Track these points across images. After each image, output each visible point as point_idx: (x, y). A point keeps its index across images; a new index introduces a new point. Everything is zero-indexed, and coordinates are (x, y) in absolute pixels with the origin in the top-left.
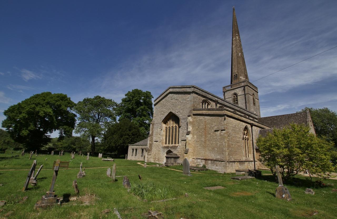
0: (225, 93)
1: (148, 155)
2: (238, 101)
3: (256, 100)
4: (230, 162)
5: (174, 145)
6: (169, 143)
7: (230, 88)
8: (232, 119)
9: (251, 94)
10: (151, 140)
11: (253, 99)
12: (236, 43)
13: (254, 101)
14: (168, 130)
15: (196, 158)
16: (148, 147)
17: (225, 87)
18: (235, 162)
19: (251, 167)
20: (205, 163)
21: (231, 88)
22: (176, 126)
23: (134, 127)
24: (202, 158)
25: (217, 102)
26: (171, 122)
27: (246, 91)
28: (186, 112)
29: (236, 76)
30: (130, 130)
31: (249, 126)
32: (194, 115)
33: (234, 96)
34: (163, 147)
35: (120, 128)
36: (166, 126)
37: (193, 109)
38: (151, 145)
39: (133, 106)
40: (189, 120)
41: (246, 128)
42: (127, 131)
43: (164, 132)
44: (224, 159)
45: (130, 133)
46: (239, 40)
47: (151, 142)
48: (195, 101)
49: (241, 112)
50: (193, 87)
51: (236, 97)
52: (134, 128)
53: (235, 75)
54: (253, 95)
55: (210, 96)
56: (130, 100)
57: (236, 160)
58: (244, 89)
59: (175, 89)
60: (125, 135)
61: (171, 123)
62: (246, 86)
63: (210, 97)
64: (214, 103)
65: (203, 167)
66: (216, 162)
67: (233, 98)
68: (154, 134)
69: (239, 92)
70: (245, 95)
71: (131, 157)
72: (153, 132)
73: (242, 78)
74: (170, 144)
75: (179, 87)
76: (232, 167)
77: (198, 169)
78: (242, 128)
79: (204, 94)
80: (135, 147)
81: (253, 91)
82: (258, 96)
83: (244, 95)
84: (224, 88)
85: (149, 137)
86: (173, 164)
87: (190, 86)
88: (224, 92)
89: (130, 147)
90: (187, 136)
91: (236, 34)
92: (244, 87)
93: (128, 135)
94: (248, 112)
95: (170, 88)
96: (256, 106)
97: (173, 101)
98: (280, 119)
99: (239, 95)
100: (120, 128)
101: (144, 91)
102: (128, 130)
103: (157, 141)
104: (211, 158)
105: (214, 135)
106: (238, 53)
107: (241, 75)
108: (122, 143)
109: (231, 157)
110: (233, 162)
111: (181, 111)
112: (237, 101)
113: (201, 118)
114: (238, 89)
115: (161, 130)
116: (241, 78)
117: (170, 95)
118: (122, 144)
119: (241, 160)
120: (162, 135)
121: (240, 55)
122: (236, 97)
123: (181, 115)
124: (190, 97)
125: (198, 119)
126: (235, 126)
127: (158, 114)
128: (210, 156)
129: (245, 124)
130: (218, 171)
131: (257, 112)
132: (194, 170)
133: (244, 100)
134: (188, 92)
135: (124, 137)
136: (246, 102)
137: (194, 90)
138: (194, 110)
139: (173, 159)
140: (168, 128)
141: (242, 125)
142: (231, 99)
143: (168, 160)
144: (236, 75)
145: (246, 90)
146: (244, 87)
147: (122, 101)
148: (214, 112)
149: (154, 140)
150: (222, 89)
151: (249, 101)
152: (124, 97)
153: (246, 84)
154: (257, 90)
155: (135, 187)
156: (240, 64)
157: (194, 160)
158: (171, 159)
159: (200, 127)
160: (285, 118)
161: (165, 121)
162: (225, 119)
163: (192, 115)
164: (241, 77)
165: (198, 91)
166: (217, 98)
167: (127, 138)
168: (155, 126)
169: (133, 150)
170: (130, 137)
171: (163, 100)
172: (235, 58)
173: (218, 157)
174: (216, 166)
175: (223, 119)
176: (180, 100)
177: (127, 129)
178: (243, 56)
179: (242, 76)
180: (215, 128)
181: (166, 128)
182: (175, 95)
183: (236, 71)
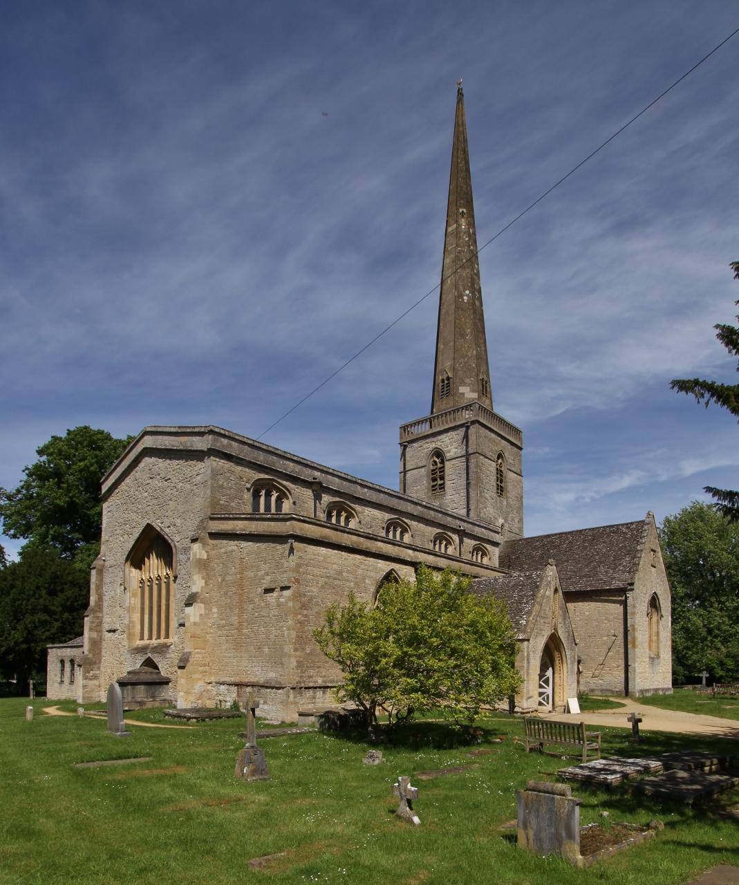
0: (405, 447)
1: (86, 678)
2: (446, 478)
3: (512, 475)
4: (306, 688)
5: (162, 640)
6: (150, 638)
7: (425, 429)
9: (489, 454)
10: (98, 627)
11: (499, 472)
12: (457, 246)
13: (500, 476)
14: (164, 585)
15: (217, 681)
16: (86, 653)
17: (407, 426)
18: (328, 687)
19: (329, 702)
20: (238, 696)
21: (431, 427)
22: (167, 574)
23: (70, 578)
24: (233, 679)
25: (318, 489)
26: (156, 561)
27: (470, 442)
28: (190, 528)
29: (446, 382)
30: (52, 593)
32: (215, 536)
33: (435, 462)
34: (133, 650)
35: (12, 586)
36: (141, 575)
37: (209, 513)
38: (96, 644)
39: (74, 496)
40: (195, 554)
42: (41, 597)
43: (134, 595)
44: (284, 681)
45: (56, 604)
46: (469, 236)
47: (95, 635)
48: (221, 487)
49: (427, 520)
50: (211, 432)
51: (439, 465)
52: (71, 582)
53: (443, 381)
54: (500, 456)
55: (291, 464)
56: (58, 475)
57: (332, 681)
58: (466, 437)
59: (160, 437)
60: (34, 611)
61: (154, 565)
62: (473, 423)
63: (291, 468)
64: (308, 493)
65: (231, 708)
66: (263, 691)
67: (432, 467)
68: (105, 604)
69: (451, 444)
70: (467, 456)
71: (56, 689)
72: (100, 598)
73: (468, 393)
74: (154, 636)
75: (173, 430)
76: (314, 703)
77: (197, 716)
78: (370, 577)
79: (261, 458)
80: (68, 653)
81: (503, 441)
82: (520, 460)
83: (464, 459)
84: (404, 428)
85: (87, 616)
86: (141, 703)
87: (203, 430)
88: (404, 446)
89: (55, 654)
90: (188, 610)
91: (461, 210)
92: (466, 426)
93: (46, 610)
94: (458, 522)
95: (146, 433)
96: (507, 498)
97: (156, 483)
98: (570, 542)
99: (448, 455)
100: (12, 586)
101: (692, 379)
102: (43, 592)
103: (114, 631)
104: (253, 679)
105: (263, 604)
106: (461, 288)
108: (21, 639)
109: (312, 672)
110: (320, 688)
111: (178, 522)
112: (442, 478)
113: (232, 545)
114: (449, 434)
115: (125, 589)
116: (463, 394)
117: (147, 461)
118: (24, 646)
119: (317, 682)
120: (130, 610)
121: (465, 298)
122: (439, 465)
123: (177, 538)
124: (202, 471)
125: (223, 550)
126: (340, 573)
127: (116, 532)
128: (250, 674)
129: (384, 566)
130: (268, 717)
131: (509, 519)
132: (185, 717)
133: (464, 476)
134: (197, 451)
135: (29, 618)
136: (468, 484)
137: (218, 446)
138: (212, 519)
139: (142, 687)
140: (146, 581)
141: (371, 568)
142: (423, 470)
143: (125, 692)
144: (448, 379)
145: (472, 438)
146: (468, 428)
147: (25, 477)
148: (264, 525)
149: (106, 627)
150: (398, 431)
151: (479, 479)
152: (34, 459)
153: (474, 419)
154: (520, 439)
156: (463, 335)
157: (209, 687)
158: (134, 689)
159: (227, 579)
160: (584, 541)
161: (136, 558)
162: (292, 550)
163: (205, 535)
164: (462, 389)
165: (235, 449)
166: (322, 471)
167: (43, 623)
168: (107, 578)
169: (62, 662)
170: (57, 617)
171: (128, 480)
172: (450, 312)
173: (272, 675)
175: (287, 552)
176: (174, 480)
177: (38, 588)
178: (477, 303)
179: (469, 385)
180: (266, 583)
181: (142, 582)
182: (161, 460)
183: (448, 364)
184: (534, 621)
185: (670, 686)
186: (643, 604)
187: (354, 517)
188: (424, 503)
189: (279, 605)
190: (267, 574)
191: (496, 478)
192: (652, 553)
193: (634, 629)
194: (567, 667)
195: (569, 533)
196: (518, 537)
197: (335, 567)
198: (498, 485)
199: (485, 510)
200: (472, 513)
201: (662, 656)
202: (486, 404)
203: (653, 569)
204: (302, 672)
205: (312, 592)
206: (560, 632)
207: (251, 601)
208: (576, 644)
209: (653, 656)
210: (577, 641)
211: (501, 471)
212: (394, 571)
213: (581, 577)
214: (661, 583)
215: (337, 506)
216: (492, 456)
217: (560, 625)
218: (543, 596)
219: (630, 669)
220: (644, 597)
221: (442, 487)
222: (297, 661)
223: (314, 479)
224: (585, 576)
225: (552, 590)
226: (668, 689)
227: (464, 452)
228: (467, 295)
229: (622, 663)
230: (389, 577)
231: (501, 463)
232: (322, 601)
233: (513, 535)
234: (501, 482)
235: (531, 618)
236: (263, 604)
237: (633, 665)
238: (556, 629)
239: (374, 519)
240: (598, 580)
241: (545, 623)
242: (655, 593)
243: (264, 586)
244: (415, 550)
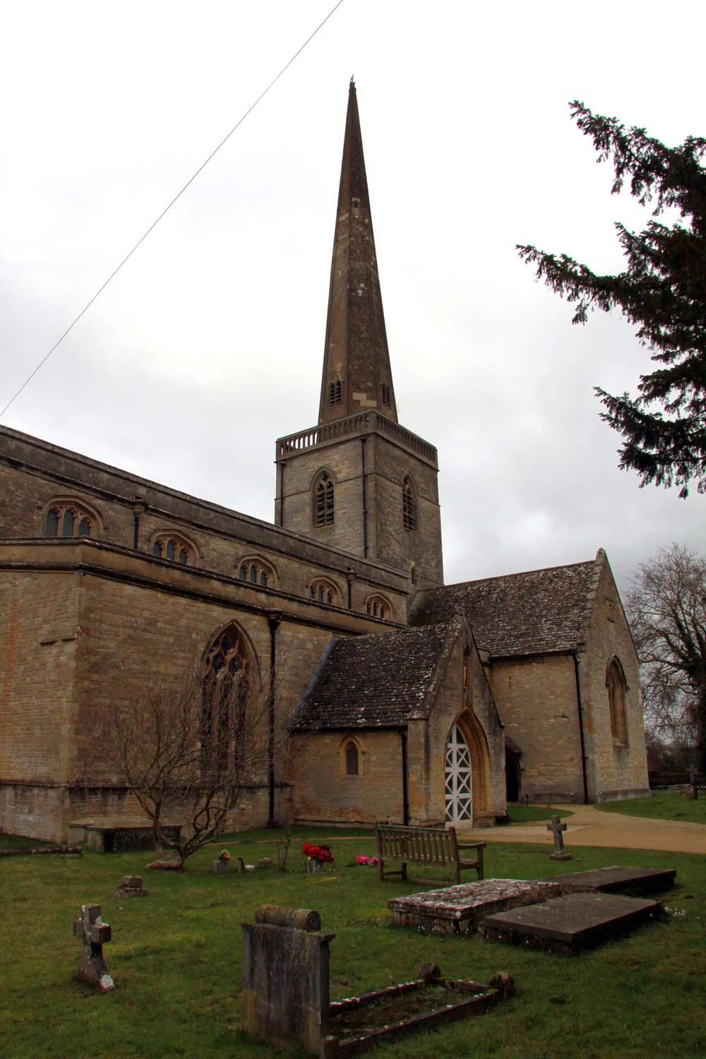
2: (336, 508)
8: (129, 589)
29: (336, 387)
31: (256, 629)
41: (231, 635)
54: (406, 480)
83: (360, 482)
99: (340, 476)
104: (17, 775)
107: (358, 387)
112: (331, 506)
116: (358, 402)
126: (152, 622)
129: (221, 616)
141: (201, 617)
144: (339, 383)
155: (128, 990)
164: (357, 396)
174: (31, 811)
180: (44, 633)
184: (435, 693)
185: (647, 786)
186: (600, 672)
187: (271, 571)
188: (297, 536)
189: (58, 666)
190: (46, 621)
191: (402, 507)
192: (608, 603)
193: (589, 707)
194: (490, 760)
195: (501, 578)
196: (435, 586)
197: (146, 614)
198: (405, 516)
199: (388, 548)
200: (371, 553)
201: (631, 744)
202: (388, 416)
203: (611, 626)
204: (85, 765)
205: (109, 648)
206: (476, 709)
207: (23, 660)
208: (502, 727)
209: (618, 744)
210: (503, 724)
211: (409, 498)
212: (238, 623)
213: (517, 637)
214: (624, 644)
215: (167, 535)
216: (396, 479)
217: (475, 700)
218: (449, 657)
219: (589, 764)
220: (601, 663)
221: (331, 518)
222: (79, 749)
223: (137, 498)
224: (523, 635)
225: (462, 650)
226: (643, 791)
227: (360, 472)
228: (362, 289)
229: (577, 755)
230: (231, 635)
231: (409, 489)
232: (123, 662)
233: (430, 583)
234: (410, 513)
235: (431, 689)
236: (37, 665)
237: (591, 757)
238: (470, 706)
239: (222, 555)
240: (540, 640)
241: (452, 695)
242: (616, 657)
243: (42, 639)
244: (224, 582)
